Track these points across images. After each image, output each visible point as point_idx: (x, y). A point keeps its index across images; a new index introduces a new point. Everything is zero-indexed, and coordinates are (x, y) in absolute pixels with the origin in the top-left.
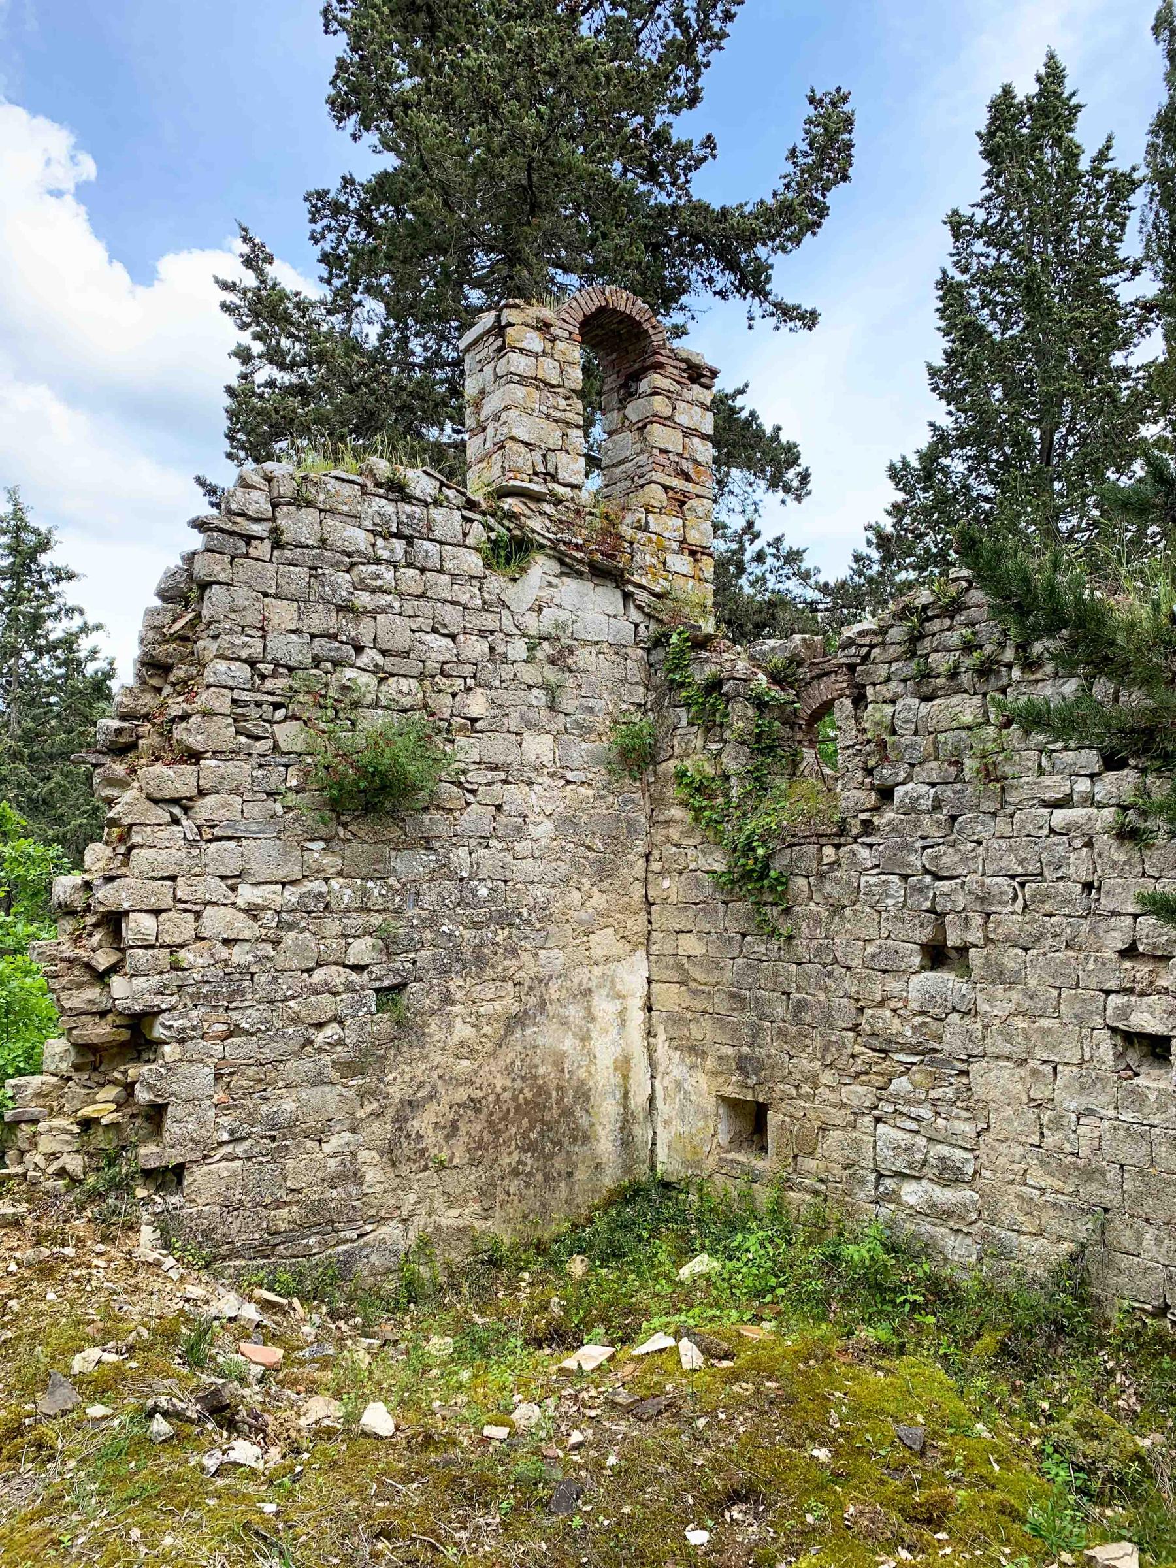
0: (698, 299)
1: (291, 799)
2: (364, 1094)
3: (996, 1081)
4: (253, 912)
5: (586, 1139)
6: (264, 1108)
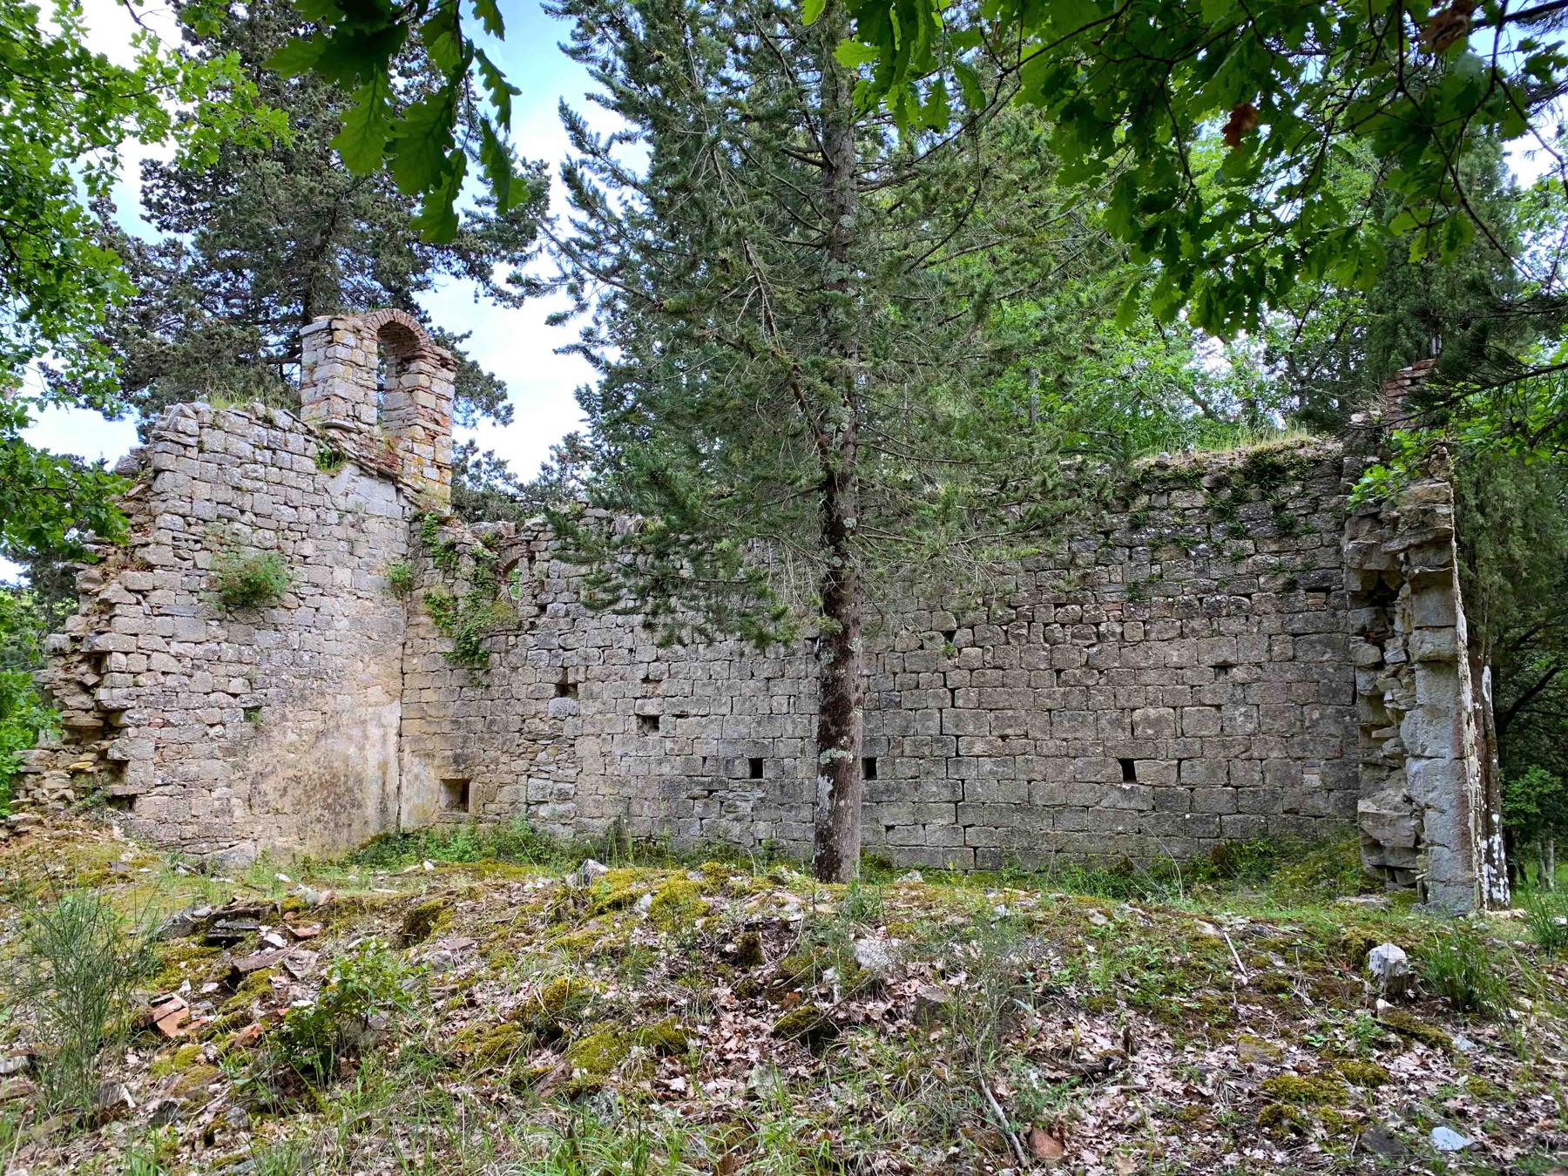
0: (440, 277)
1: (202, 594)
2: (235, 766)
3: (587, 747)
4: (178, 657)
5: (360, 806)
6: (180, 769)
